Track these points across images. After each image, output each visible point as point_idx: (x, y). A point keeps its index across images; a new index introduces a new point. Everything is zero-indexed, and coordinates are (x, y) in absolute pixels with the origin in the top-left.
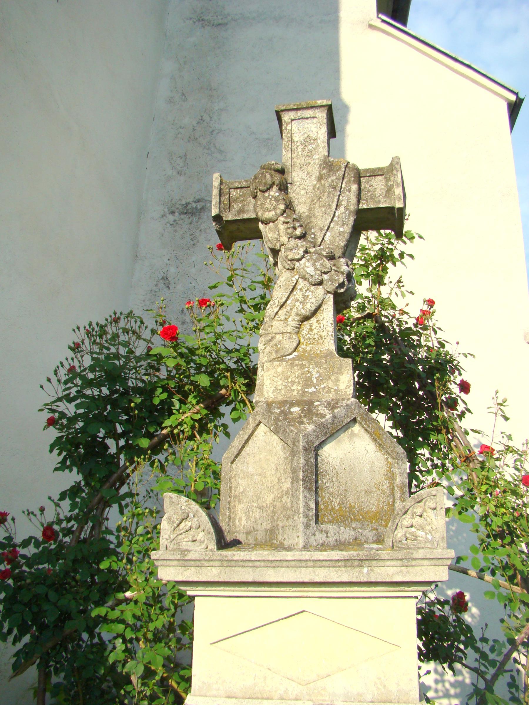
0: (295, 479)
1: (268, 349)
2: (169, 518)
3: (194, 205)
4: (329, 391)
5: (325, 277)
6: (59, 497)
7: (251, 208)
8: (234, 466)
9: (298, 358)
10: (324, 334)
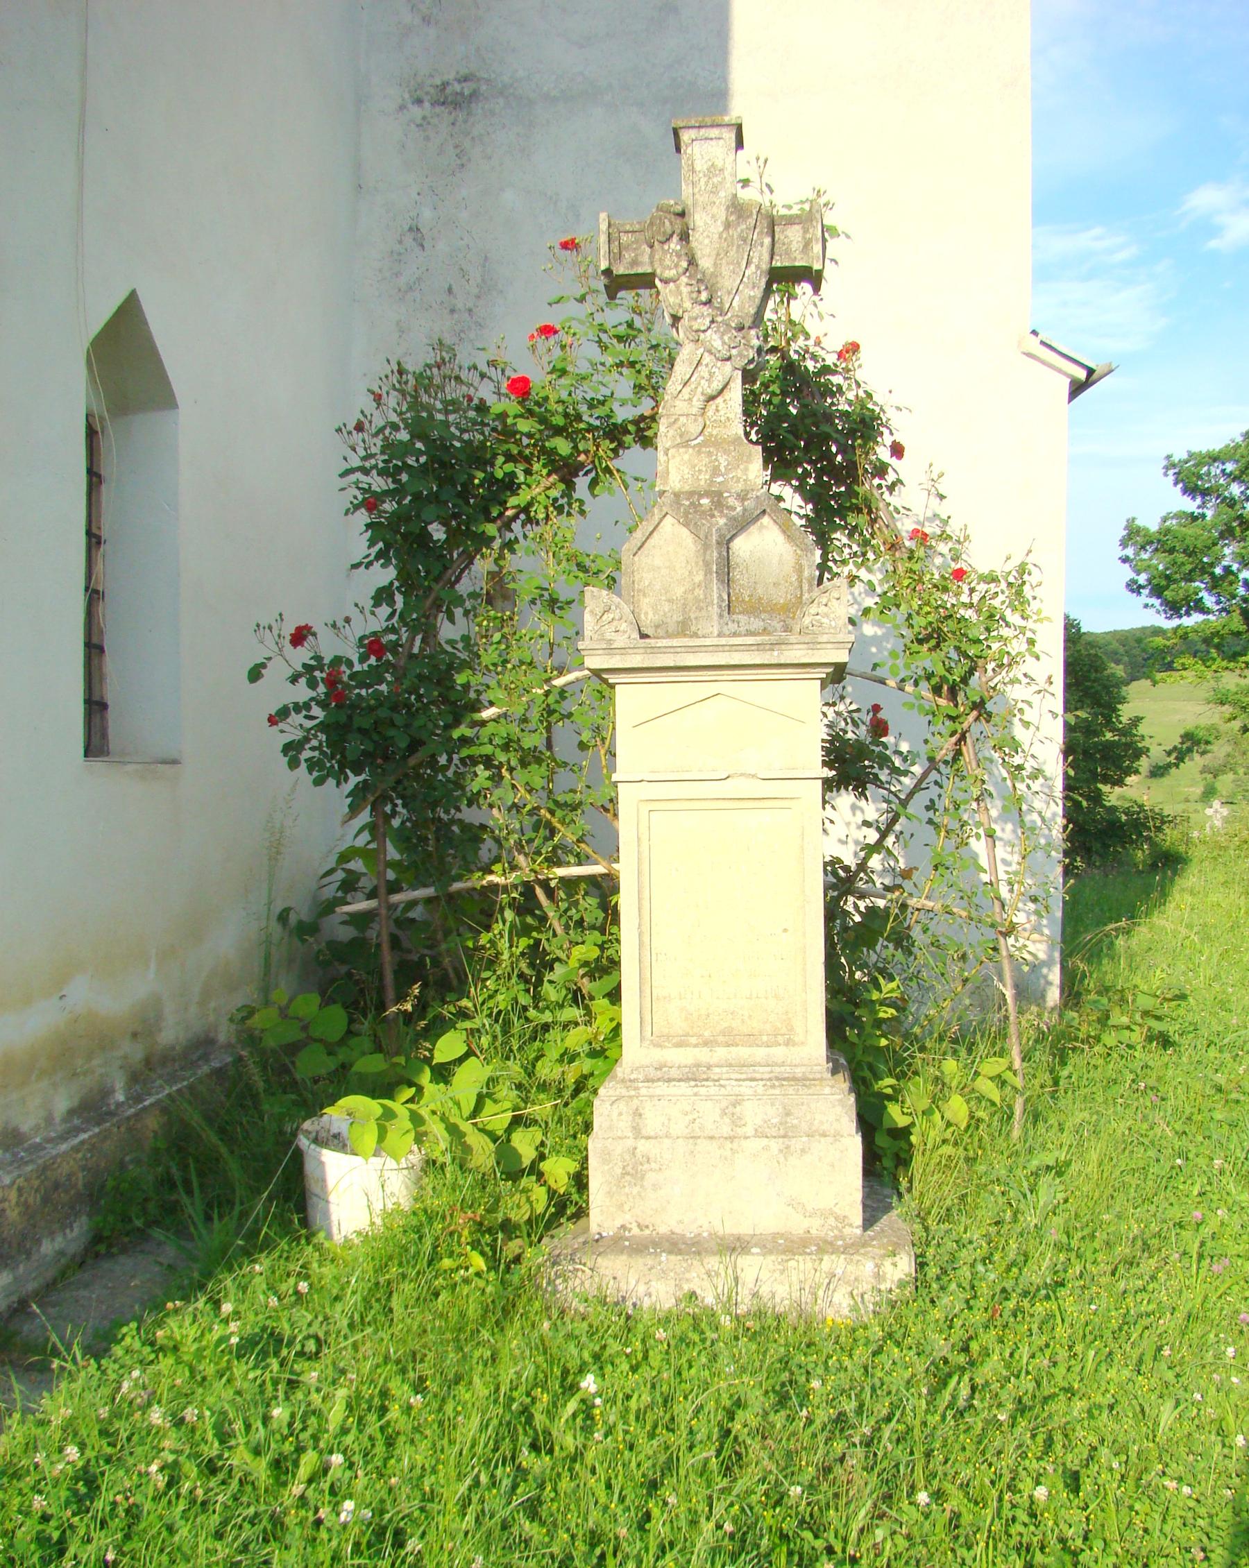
0: (708, 572)
1: (671, 432)
2: (591, 612)
3: (457, 87)
4: (738, 481)
5: (734, 352)
6: (372, 602)
7: (646, 259)
8: (636, 558)
9: (705, 444)
10: (731, 416)
